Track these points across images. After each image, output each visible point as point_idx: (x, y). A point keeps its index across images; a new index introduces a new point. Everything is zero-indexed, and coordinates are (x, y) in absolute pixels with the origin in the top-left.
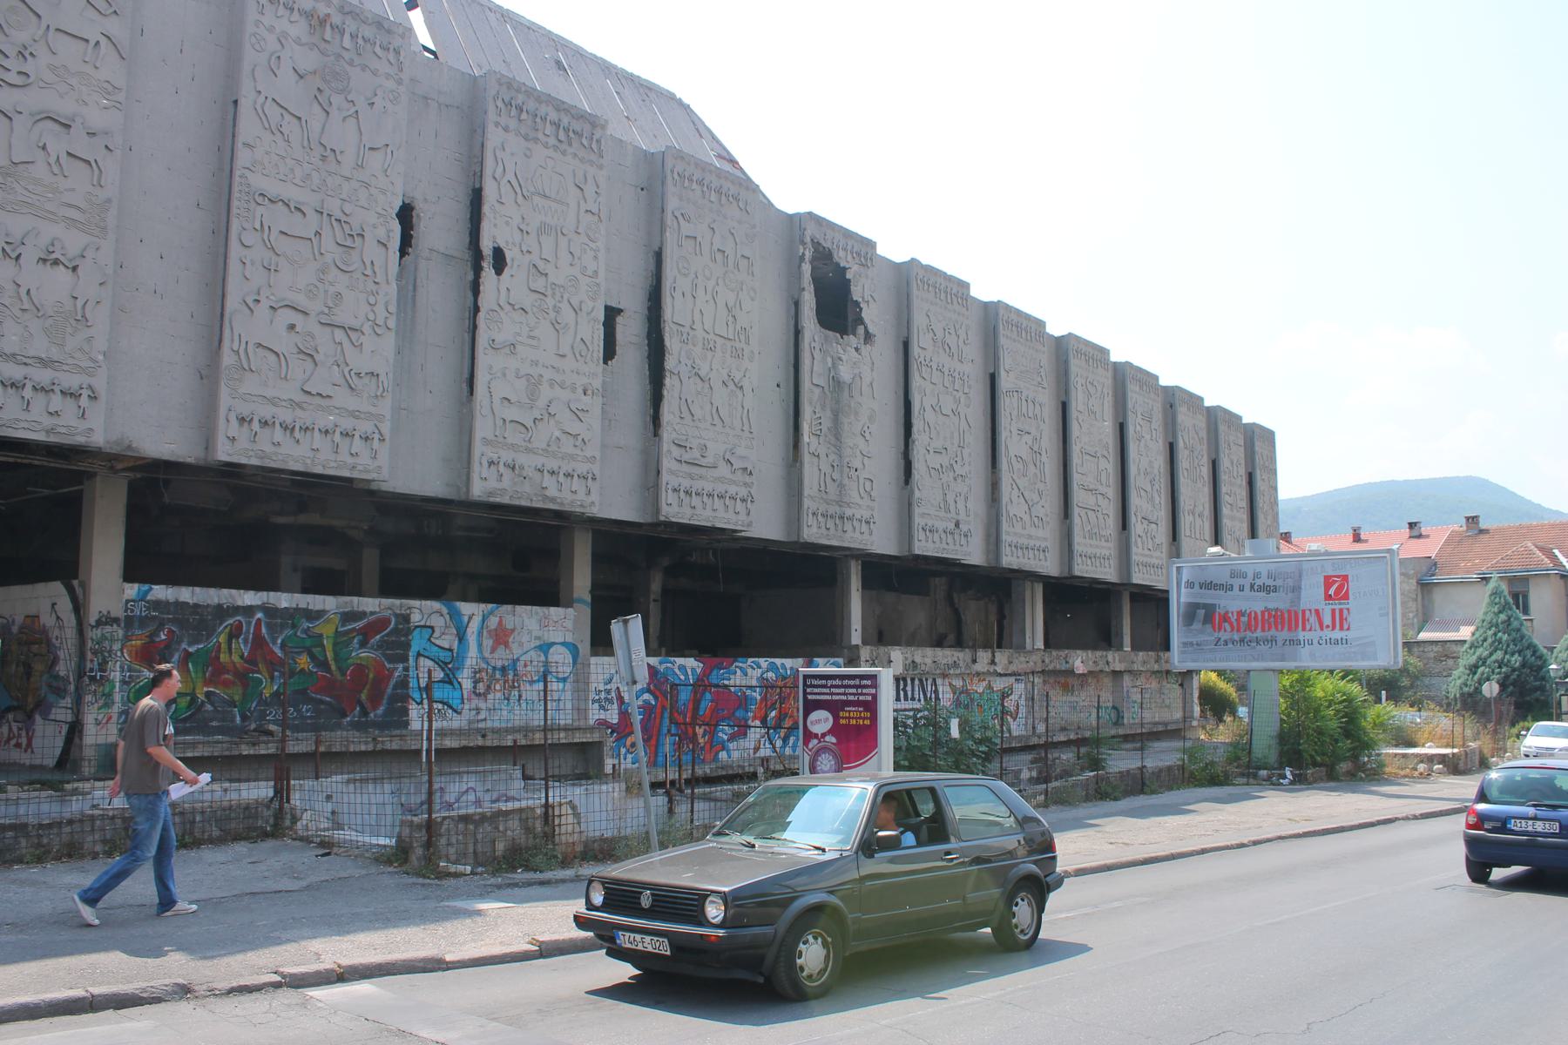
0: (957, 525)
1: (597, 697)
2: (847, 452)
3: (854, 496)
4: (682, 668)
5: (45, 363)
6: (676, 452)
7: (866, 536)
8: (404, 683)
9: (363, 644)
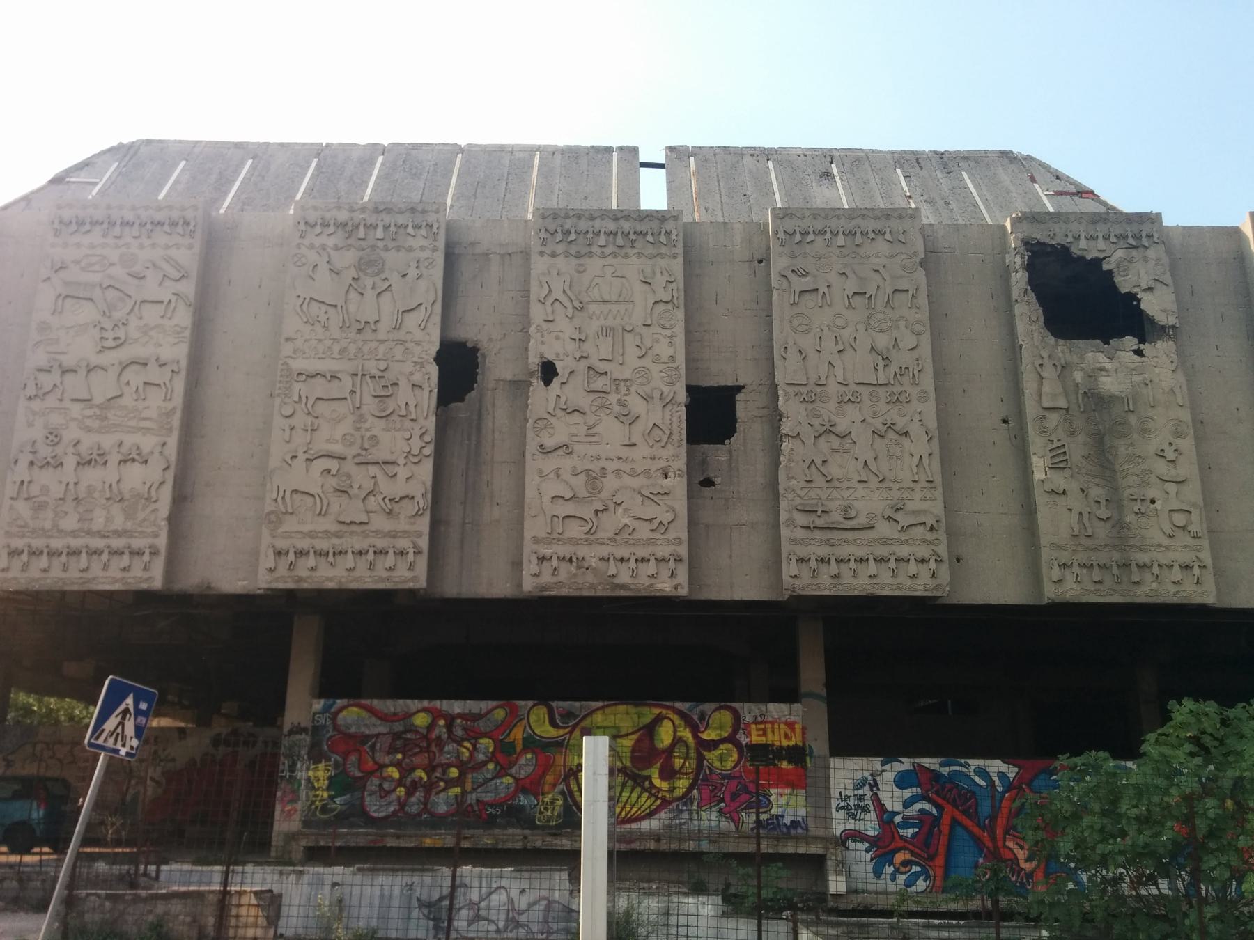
1: (843, 804)
6: (801, 519)
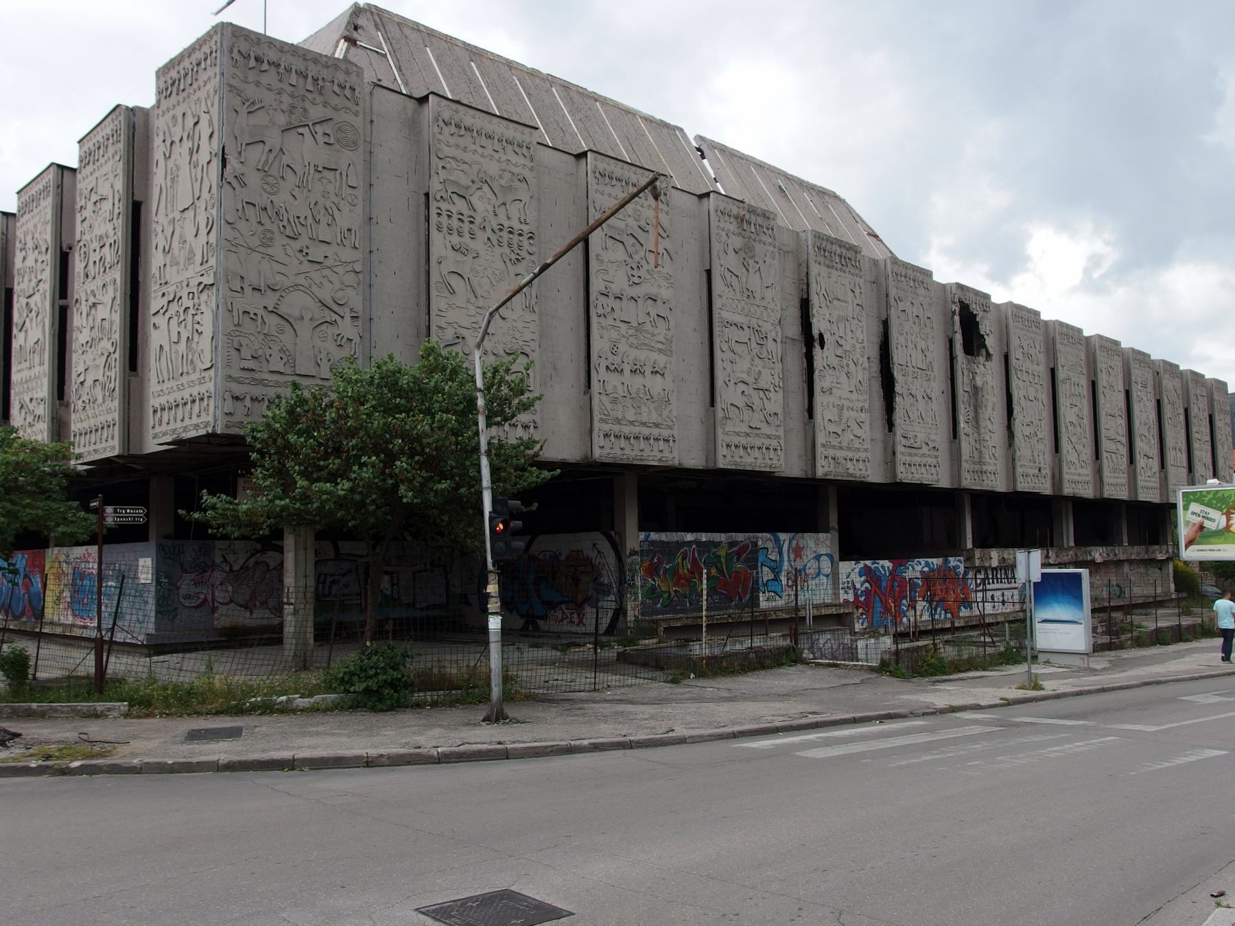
0: (1040, 470)
2: (982, 431)
3: (987, 458)
4: (883, 567)
5: (657, 425)
6: (904, 441)
7: (994, 483)
8: (756, 582)
9: (738, 560)
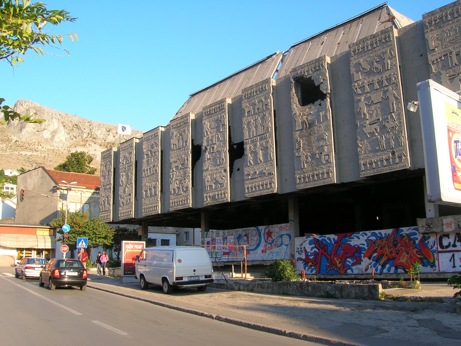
4: (329, 239)
